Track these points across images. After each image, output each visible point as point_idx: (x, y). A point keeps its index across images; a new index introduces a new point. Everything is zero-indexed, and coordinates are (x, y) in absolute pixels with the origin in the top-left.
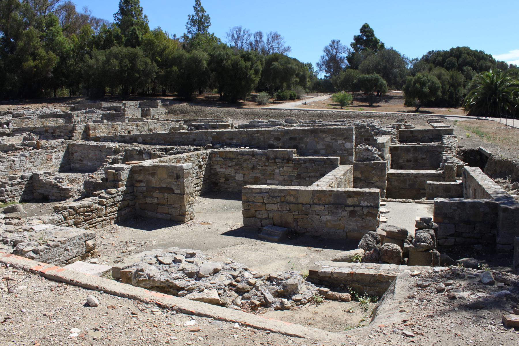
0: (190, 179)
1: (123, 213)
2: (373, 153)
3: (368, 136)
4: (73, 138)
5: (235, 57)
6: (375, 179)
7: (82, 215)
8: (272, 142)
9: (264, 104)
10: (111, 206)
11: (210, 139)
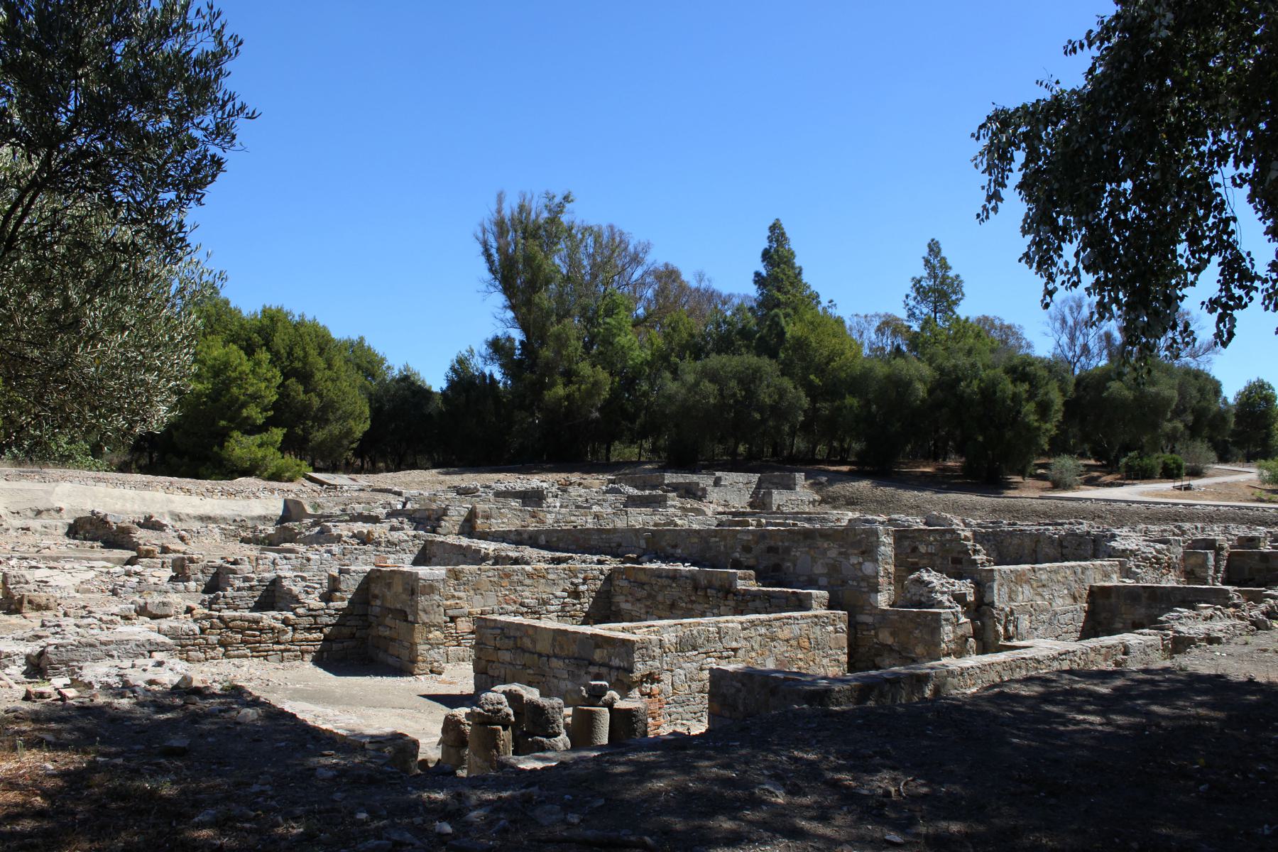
0: (437, 597)
1: (335, 646)
2: (932, 590)
3: (959, 552)
4: (439, 530)
5: (990, 372)
6: (919, 650)
7: (238, 633)
8: (737, 555)
9: (1067, 487)
10: (309, 630)
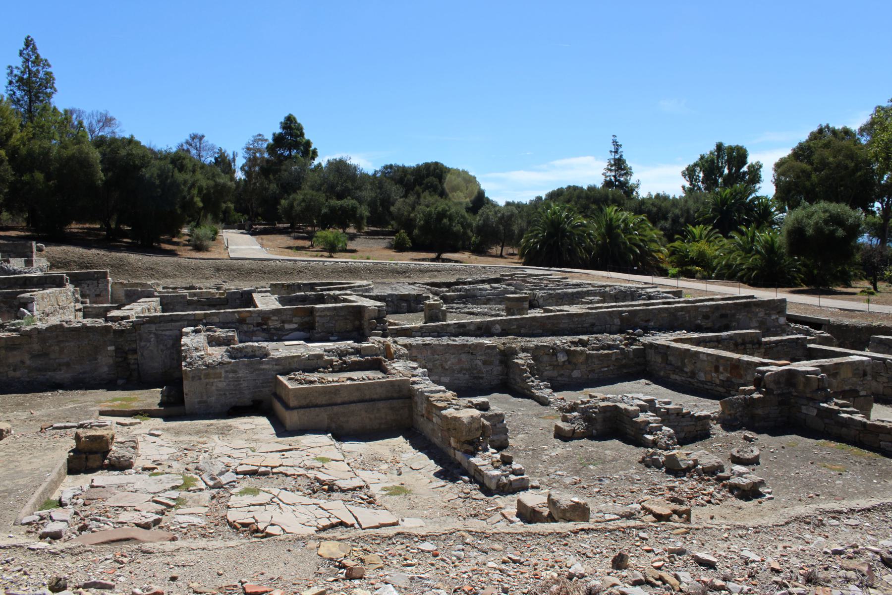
11: (617, 321)
